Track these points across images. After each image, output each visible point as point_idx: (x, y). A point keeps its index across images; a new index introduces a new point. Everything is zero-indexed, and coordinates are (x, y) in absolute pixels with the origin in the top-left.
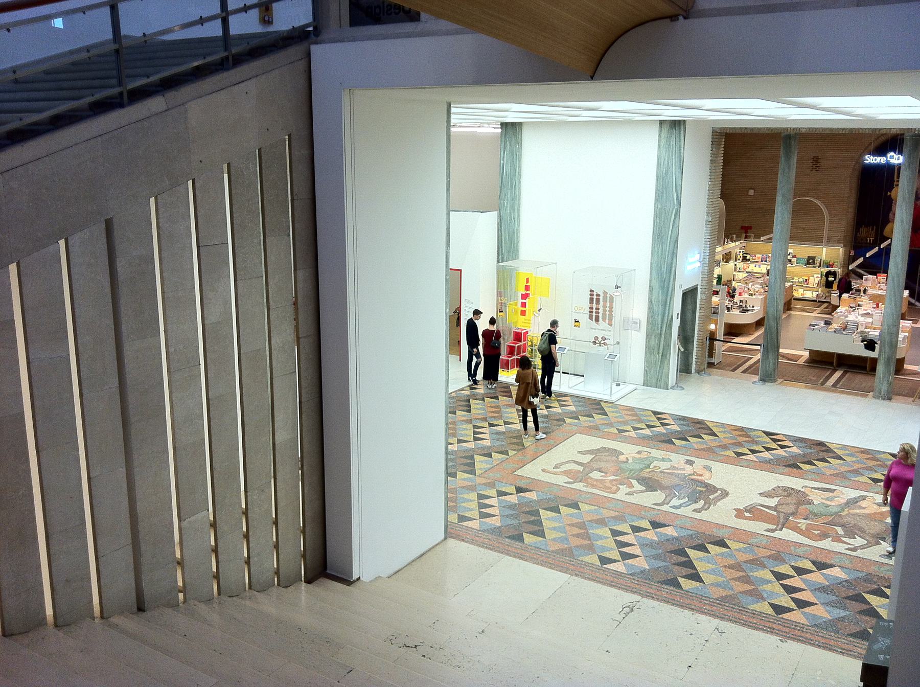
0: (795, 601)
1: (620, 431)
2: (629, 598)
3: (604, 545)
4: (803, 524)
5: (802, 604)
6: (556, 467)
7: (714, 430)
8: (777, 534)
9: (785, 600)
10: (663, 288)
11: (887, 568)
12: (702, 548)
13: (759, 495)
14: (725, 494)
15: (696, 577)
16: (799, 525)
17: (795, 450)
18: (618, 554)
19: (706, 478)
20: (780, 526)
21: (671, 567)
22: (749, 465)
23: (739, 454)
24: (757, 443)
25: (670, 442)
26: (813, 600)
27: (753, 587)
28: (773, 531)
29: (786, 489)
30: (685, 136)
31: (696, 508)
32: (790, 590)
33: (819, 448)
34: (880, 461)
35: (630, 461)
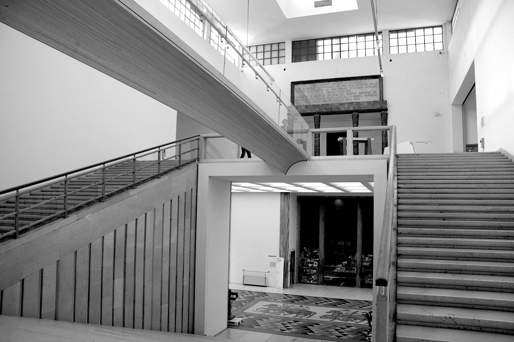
1: (275, 300)
2: (293, 338)
4: (341, 318)
5: (345, 335)
6: (257, 310)
7: (307, 298)
9: (340, 335)
10: (284, 251)
11: (367, 326)
12: (312, 325)
14: (315, 313)
15: (312, 332)
19: (308, 310)
20: (334, 319)
22: (320, 306)
24: (322, 301)
26: (347, 334)
28: (332, 320)
29: (334, 311)
30: (289, 197)
32: (340, 332)
33: (342, 301)
35: (282, 307)
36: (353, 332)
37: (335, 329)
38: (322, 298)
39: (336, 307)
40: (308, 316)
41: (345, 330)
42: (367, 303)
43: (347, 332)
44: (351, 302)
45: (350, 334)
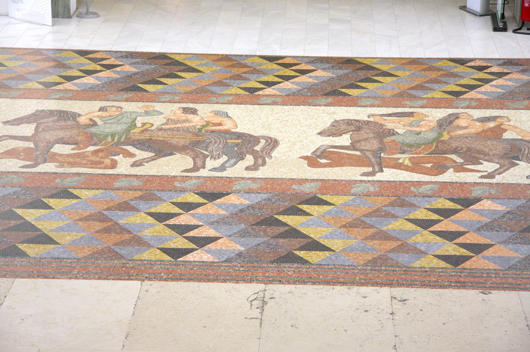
0: (192, 239)
3: (155, 234)
4: (404, 158)
7: (189, 63)
8: (379, 177)
9: (180, 243)
13: (319, 136)
14: (273, 143)
15: (46, 240)
16: (401, 161)
17: (128, 68)
18: (187, 241)
21: (271, 241)
23: (252, 90)
25: (135, 89)
27: (400, 243)
28: (373, 174)
31: (247, 165)
32: (182, 230)
34: (442, 70)
36: (500, 227)
37: (153, 210)
38: (256, 59)
39: (140, 94)
40: (249, 160)
41: (200, 217)
42: (275, 66)
43: (475, 231)
44: (11, 59)
45: (500, 243)
